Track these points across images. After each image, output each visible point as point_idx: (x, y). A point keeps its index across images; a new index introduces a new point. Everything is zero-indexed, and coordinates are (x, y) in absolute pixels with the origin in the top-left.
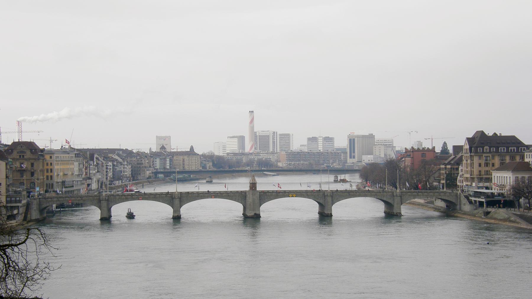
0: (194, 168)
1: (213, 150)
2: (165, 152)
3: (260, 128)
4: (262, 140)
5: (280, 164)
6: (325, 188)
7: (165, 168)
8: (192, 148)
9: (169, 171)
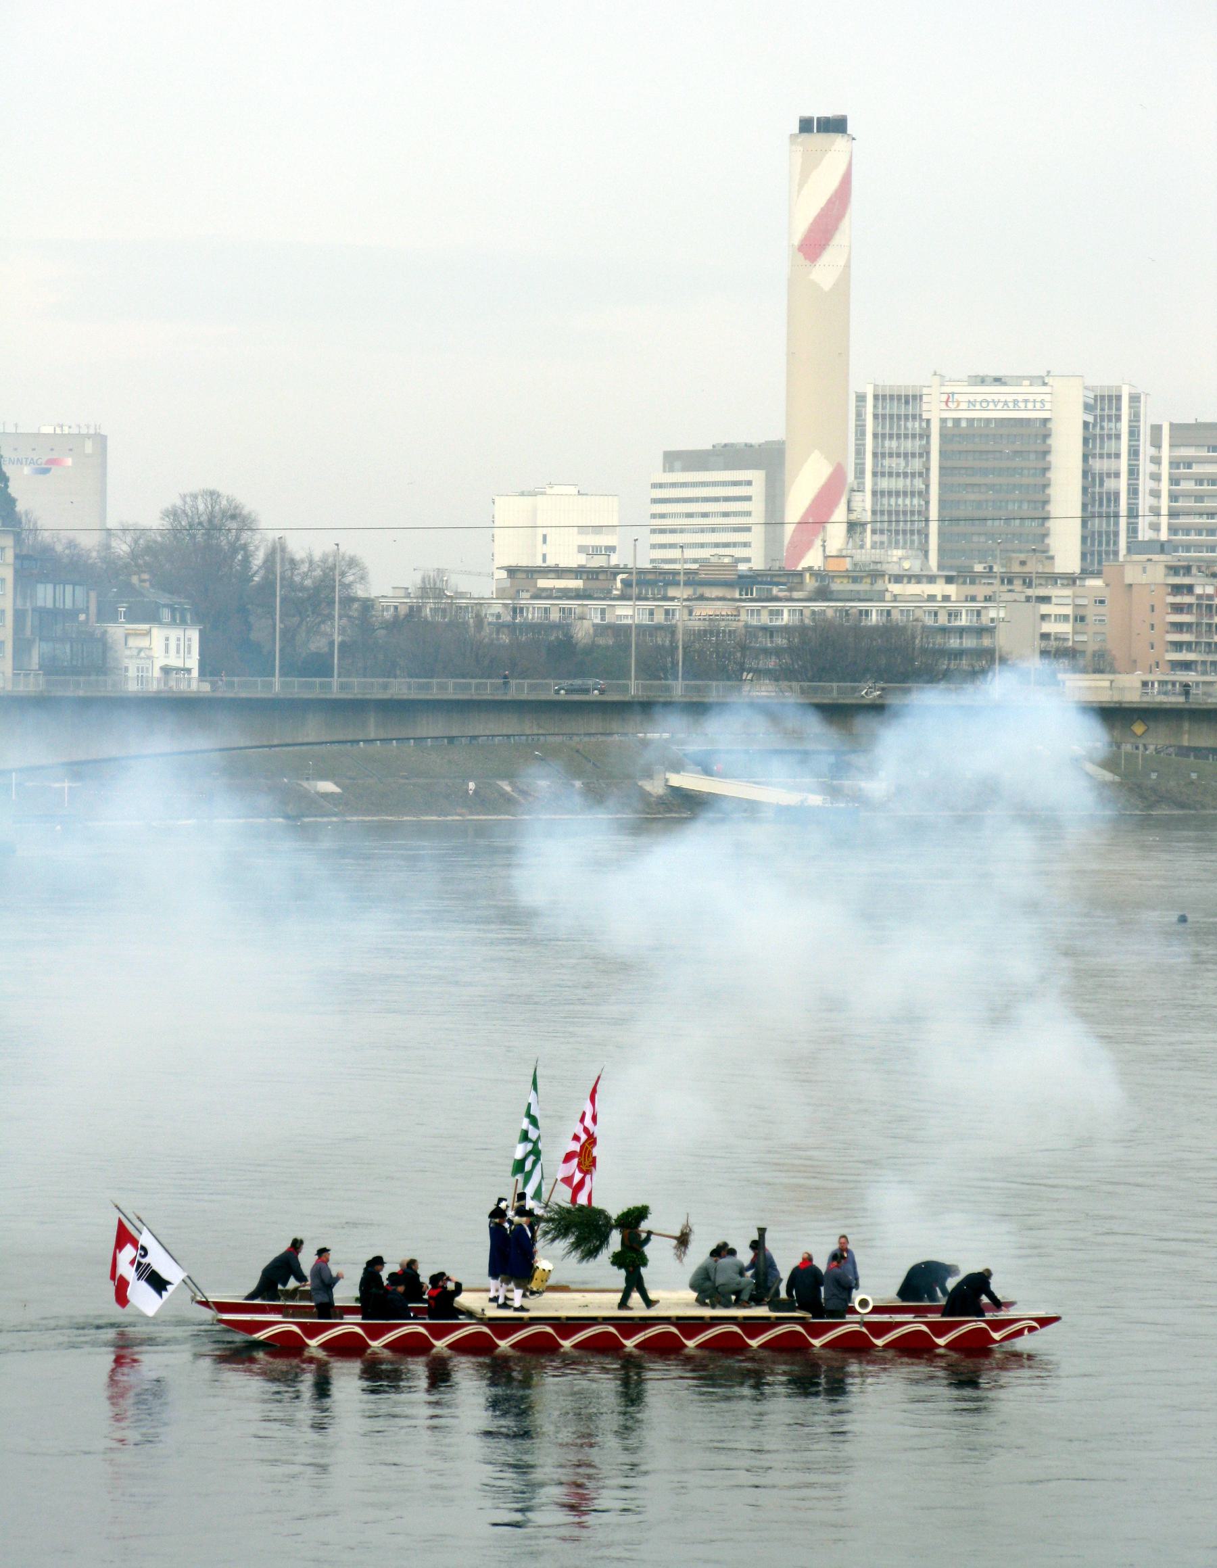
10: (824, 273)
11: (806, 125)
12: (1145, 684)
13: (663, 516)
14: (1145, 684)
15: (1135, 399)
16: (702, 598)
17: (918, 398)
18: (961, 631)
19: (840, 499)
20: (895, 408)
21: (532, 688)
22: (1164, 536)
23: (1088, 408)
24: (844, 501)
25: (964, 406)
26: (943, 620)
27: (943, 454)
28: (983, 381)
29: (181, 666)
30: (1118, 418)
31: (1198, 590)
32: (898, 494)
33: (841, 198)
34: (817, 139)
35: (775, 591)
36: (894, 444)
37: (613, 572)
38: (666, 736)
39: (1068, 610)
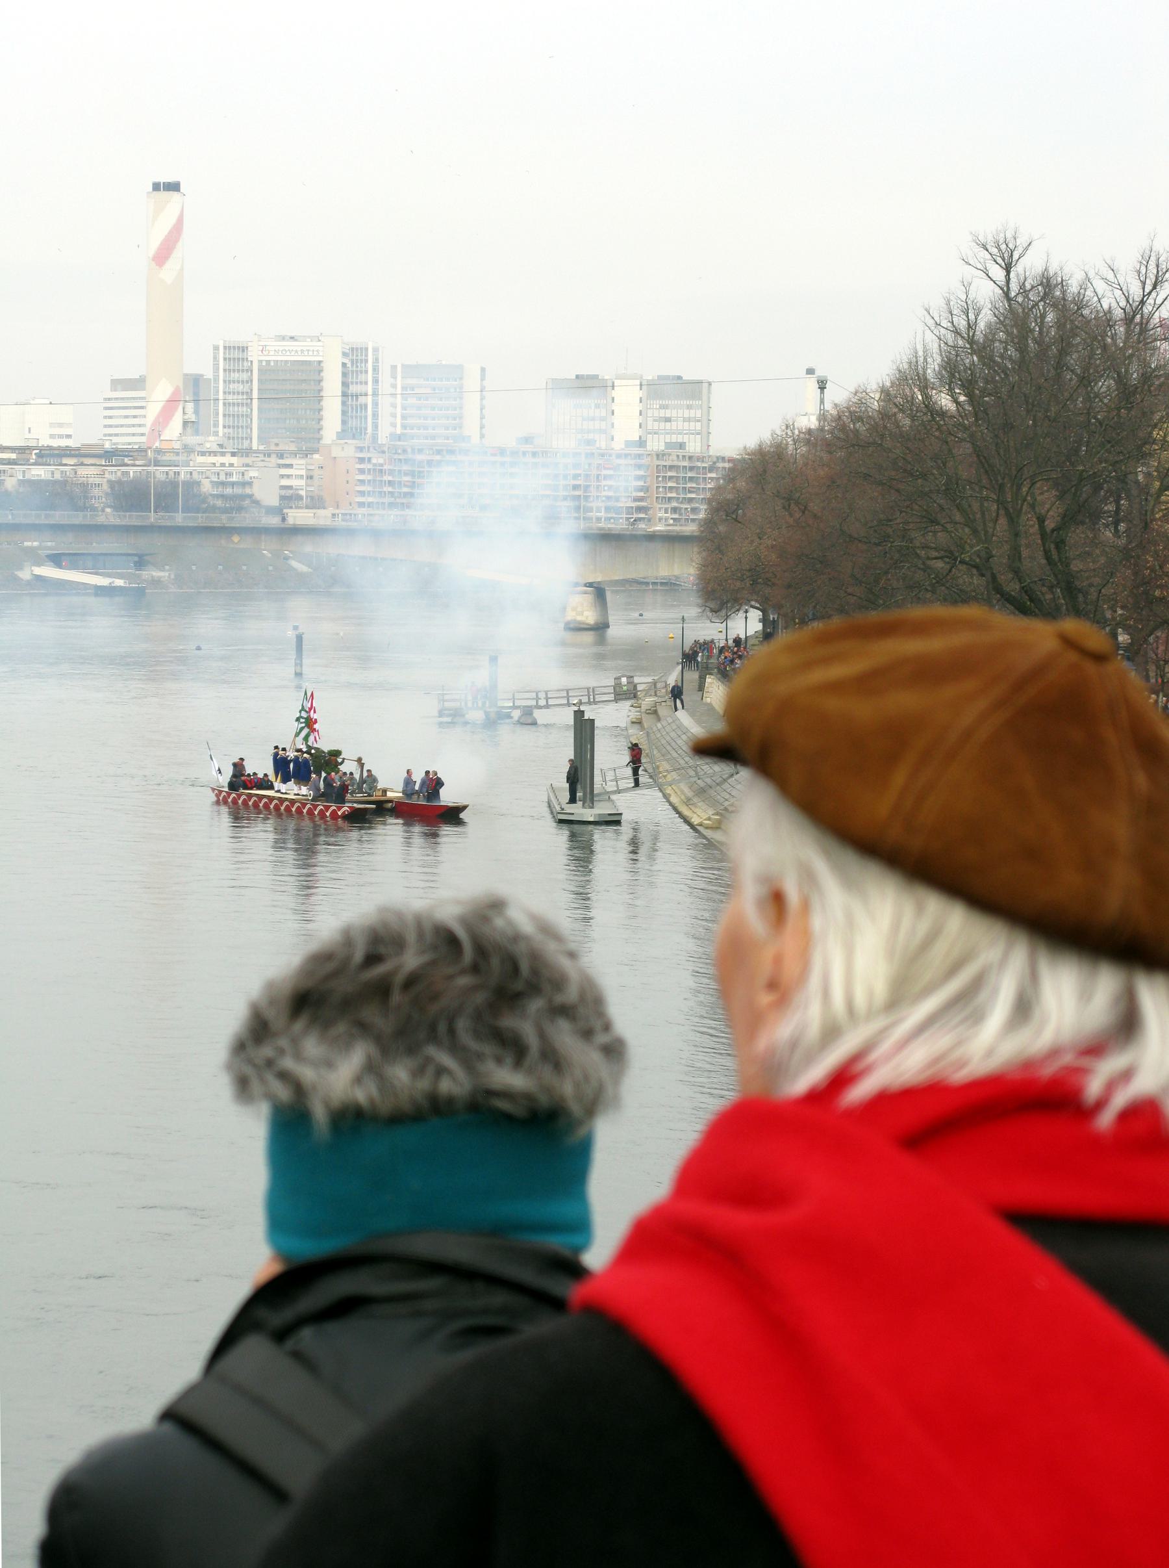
10: (168, 273)
12: (334, 515)
13: (110, 417)
14: (334, 515)
15: (376, 350)
16: (82, 464)
17: (244, 349)
18: (233, 484)
20: (236, 354)
21: (47, 516)
22: (399, 431)
23: (345, 354)
26: (222, 477)
27: (260, 380)
28: (283, 338)
30: (366, 361)
31: (374, 461)
32: (238, 404)
33: (177, 229)
34: (163, 195)
35: (126, 460)
36: (237, 375)
37: (30, 448)
38: (36, 544)
39: (303, 472)
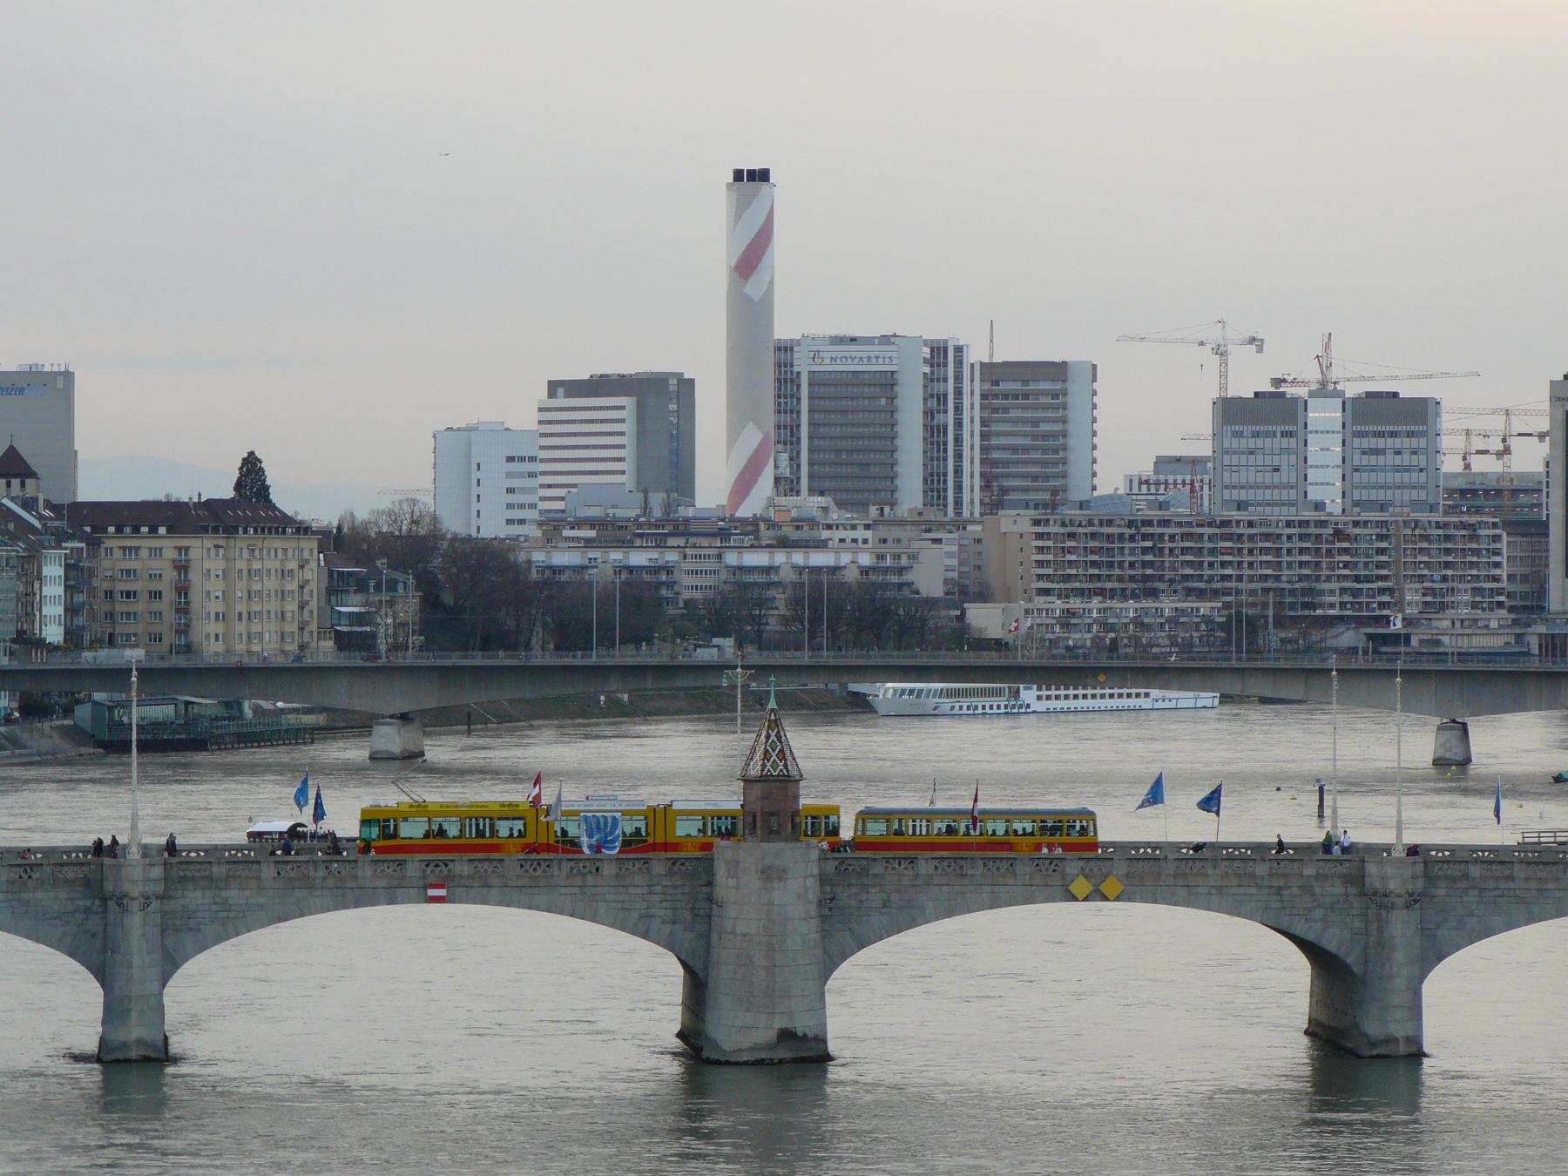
0: (267, 642)
1: (427, 502)
2: (29, 504)
3: (814, 306)
4: (834, 414)
5: (985, 619)
6: (1367, 823)
7: (26, 640)
8: (251, 469)
9: (59, 662)
10: (754, 288)
11: (738, 175)
19: (765, 464)
24: (771, 463)
25: (827, 361)
29: (925, 805)
